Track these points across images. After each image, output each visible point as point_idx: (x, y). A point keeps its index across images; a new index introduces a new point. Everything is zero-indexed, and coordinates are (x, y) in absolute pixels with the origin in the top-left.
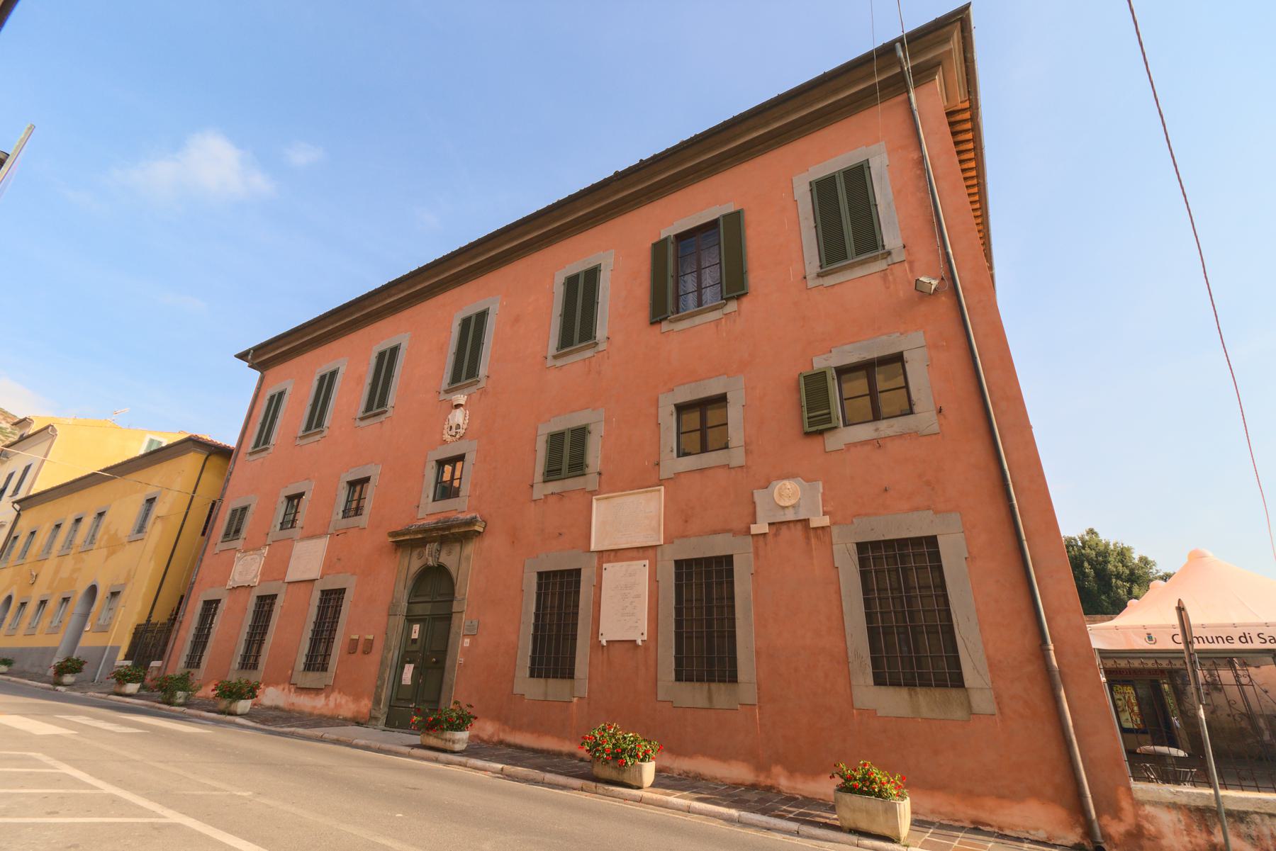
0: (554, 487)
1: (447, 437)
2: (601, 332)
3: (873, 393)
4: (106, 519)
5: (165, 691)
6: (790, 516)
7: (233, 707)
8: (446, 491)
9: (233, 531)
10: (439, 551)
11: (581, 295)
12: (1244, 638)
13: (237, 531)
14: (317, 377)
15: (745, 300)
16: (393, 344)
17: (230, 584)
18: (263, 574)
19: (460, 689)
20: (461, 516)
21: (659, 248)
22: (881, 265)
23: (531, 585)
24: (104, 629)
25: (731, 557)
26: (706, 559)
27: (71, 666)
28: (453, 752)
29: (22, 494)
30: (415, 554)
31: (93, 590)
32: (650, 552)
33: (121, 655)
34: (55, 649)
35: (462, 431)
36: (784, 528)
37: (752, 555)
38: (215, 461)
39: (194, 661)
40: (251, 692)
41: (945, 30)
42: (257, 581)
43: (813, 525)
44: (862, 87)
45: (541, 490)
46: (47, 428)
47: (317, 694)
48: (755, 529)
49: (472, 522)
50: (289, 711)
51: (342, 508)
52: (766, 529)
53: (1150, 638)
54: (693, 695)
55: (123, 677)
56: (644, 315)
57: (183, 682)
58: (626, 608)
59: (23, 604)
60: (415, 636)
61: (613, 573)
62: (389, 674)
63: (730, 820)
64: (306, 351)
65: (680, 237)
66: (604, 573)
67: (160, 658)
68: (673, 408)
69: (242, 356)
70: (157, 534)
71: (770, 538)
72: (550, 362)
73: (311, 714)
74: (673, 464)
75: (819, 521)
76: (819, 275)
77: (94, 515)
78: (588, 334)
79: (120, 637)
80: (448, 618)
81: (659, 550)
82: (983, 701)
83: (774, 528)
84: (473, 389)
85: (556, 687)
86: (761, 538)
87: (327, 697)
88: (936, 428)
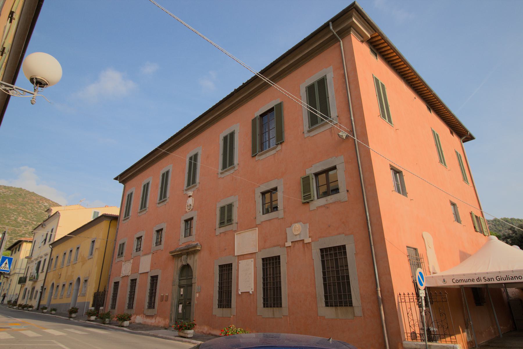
0: (223, 229)
1: (187, 210)
2: (236, 161)
4: (80, 250)
5: (102, 319)
7: (123, 324)
8: (188, 232)
9: (121, 254)
10: (187, 258)
12: (479, 279)
13: (122, 253)
14: (161, 175)
15: (283, 144)
16: (195, 153)
17: (122, 275)
18: (132, 271)
19: (196, 314)
21: (254, 121)
23: (217, 269)
24: (84, 295)
25: (279, 256)
26: (334, 247)
27: (74, 311)
28: (188, 338)
29: (52, 242)
30: (179, 260)
31: (79, 279)
32: (254, 256)
33: (91, 305)
34: (70, 303)
35: (192, 207)
36: (296, 243)
37: (286, 256)
38: (113, 222)
39: (113, 307)
40: (129, 318)
41: (349, 13)
42: (130, 273)
43: (305, 242)
44: (321, 41)
45: (219, 231)
46: (56, 213)
47: (152, 318)
49: (195, 246)
50: (144, 325)
51: (155, 242)
53: (444, 281)
54: (268, 312)
55: (90, 314)
56: (250, 153)
57: (108, 315)
59: (58, 286)
60: (182, 293)
62: (174, 309)
64: (149, 167)
65: (262, 116)
66: (240, 265)
67: (103, 306)
68: (260, 194)
69: (116, 179)
70: (97, 255)
71: (292, 247)
72: (306, 135)
73: (151, 326)
74: (262, 218)
75: (308, 240)
76: (309, 131)
77: (76, 249)
78: (231, 163)
79: (89, 298)
80: (191, 285)
81: (257, 254)
82: (358, 311)
83: (293, 243)
84: (194, 189)
85: (226, 311)
87: (155, 319)
88: (346, 199)
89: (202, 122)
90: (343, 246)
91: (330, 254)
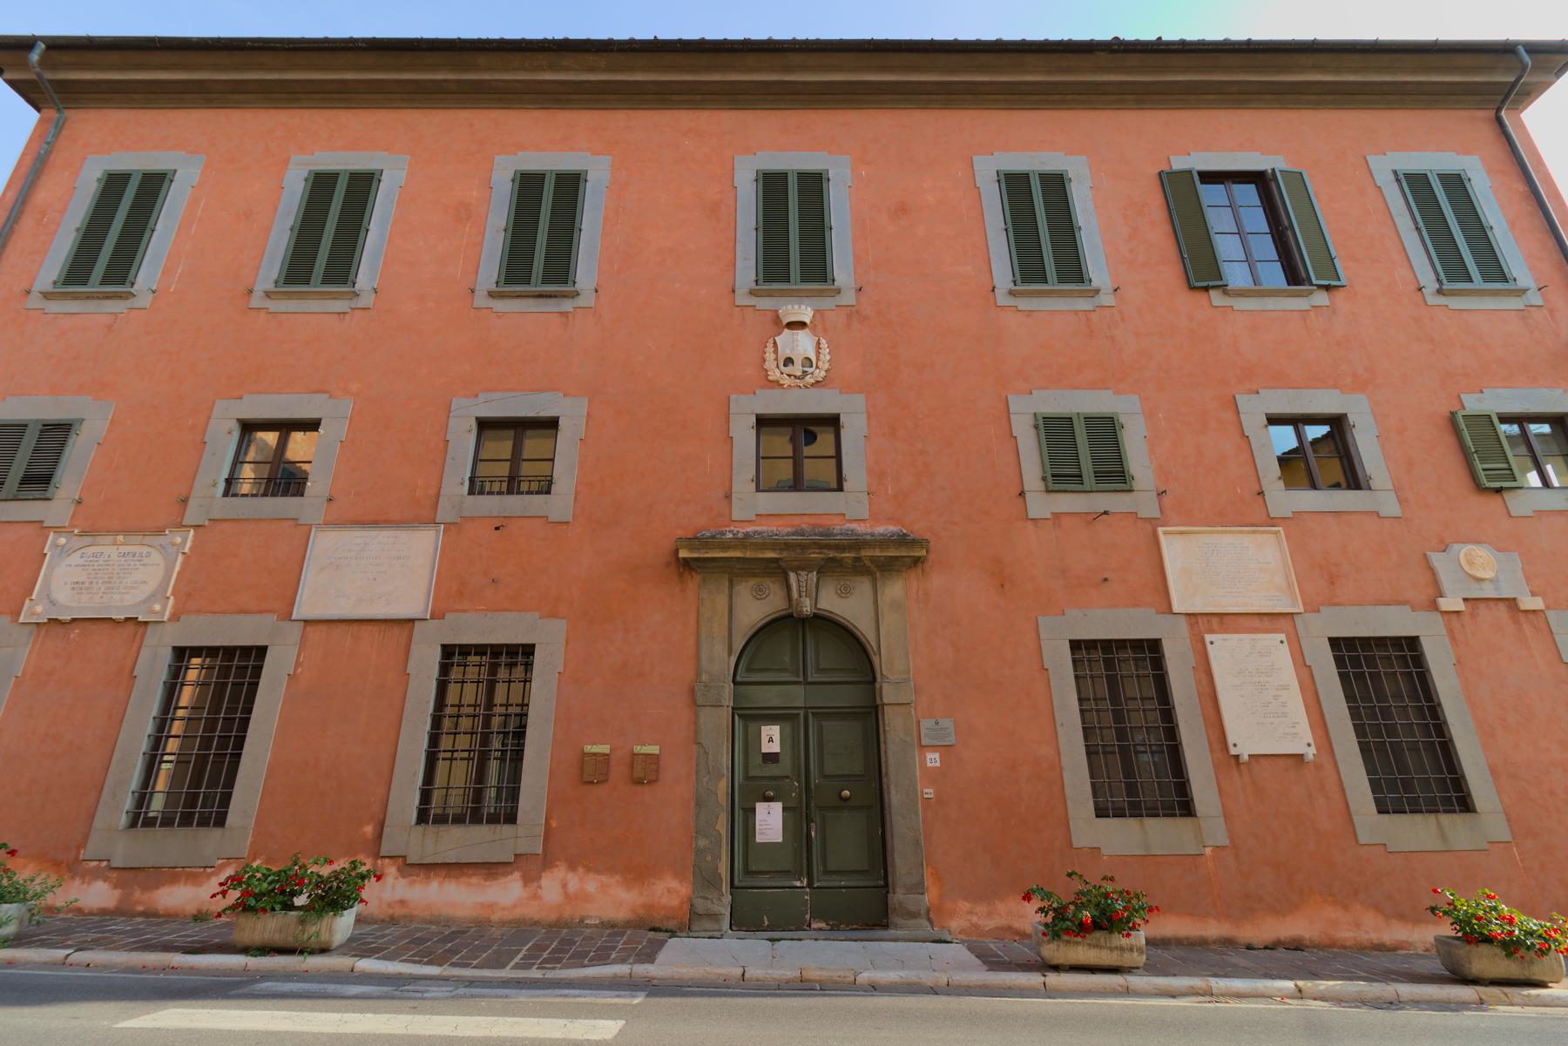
0: (1068, 502)
3: (516, 459)
6: (1489, 592)
11: (127, 208)
17: (36, 610)
20: (860, 528)
22: (1082, 304)
36: (1482, 606)
48: (1445, 604)
52: (1461, 607)
58: (1264, 704)
61: (1224, 649)
63: (1338, 1000)
64: (237, 105)
72: (254, 303)
76: (752, 293)
78: (121, 271)
81: (150, 628)
86: (1454, 617)
87: (528, 880)
89: (553, 68)
90: (524, 646)
91: (1089, 660)
